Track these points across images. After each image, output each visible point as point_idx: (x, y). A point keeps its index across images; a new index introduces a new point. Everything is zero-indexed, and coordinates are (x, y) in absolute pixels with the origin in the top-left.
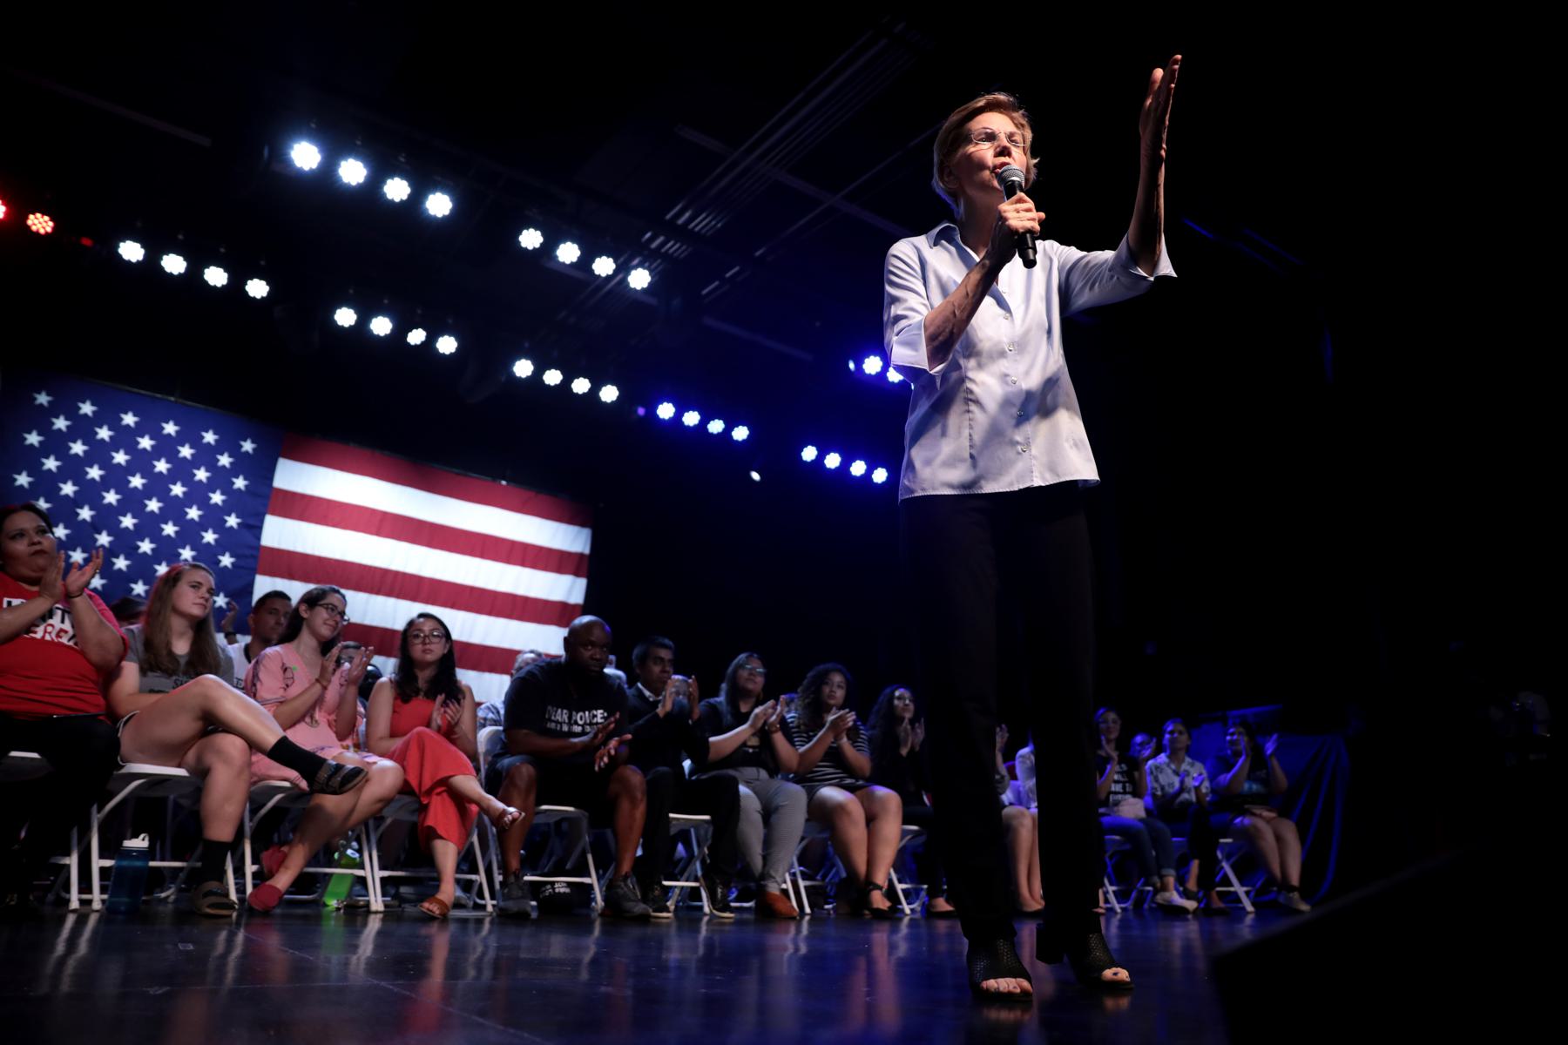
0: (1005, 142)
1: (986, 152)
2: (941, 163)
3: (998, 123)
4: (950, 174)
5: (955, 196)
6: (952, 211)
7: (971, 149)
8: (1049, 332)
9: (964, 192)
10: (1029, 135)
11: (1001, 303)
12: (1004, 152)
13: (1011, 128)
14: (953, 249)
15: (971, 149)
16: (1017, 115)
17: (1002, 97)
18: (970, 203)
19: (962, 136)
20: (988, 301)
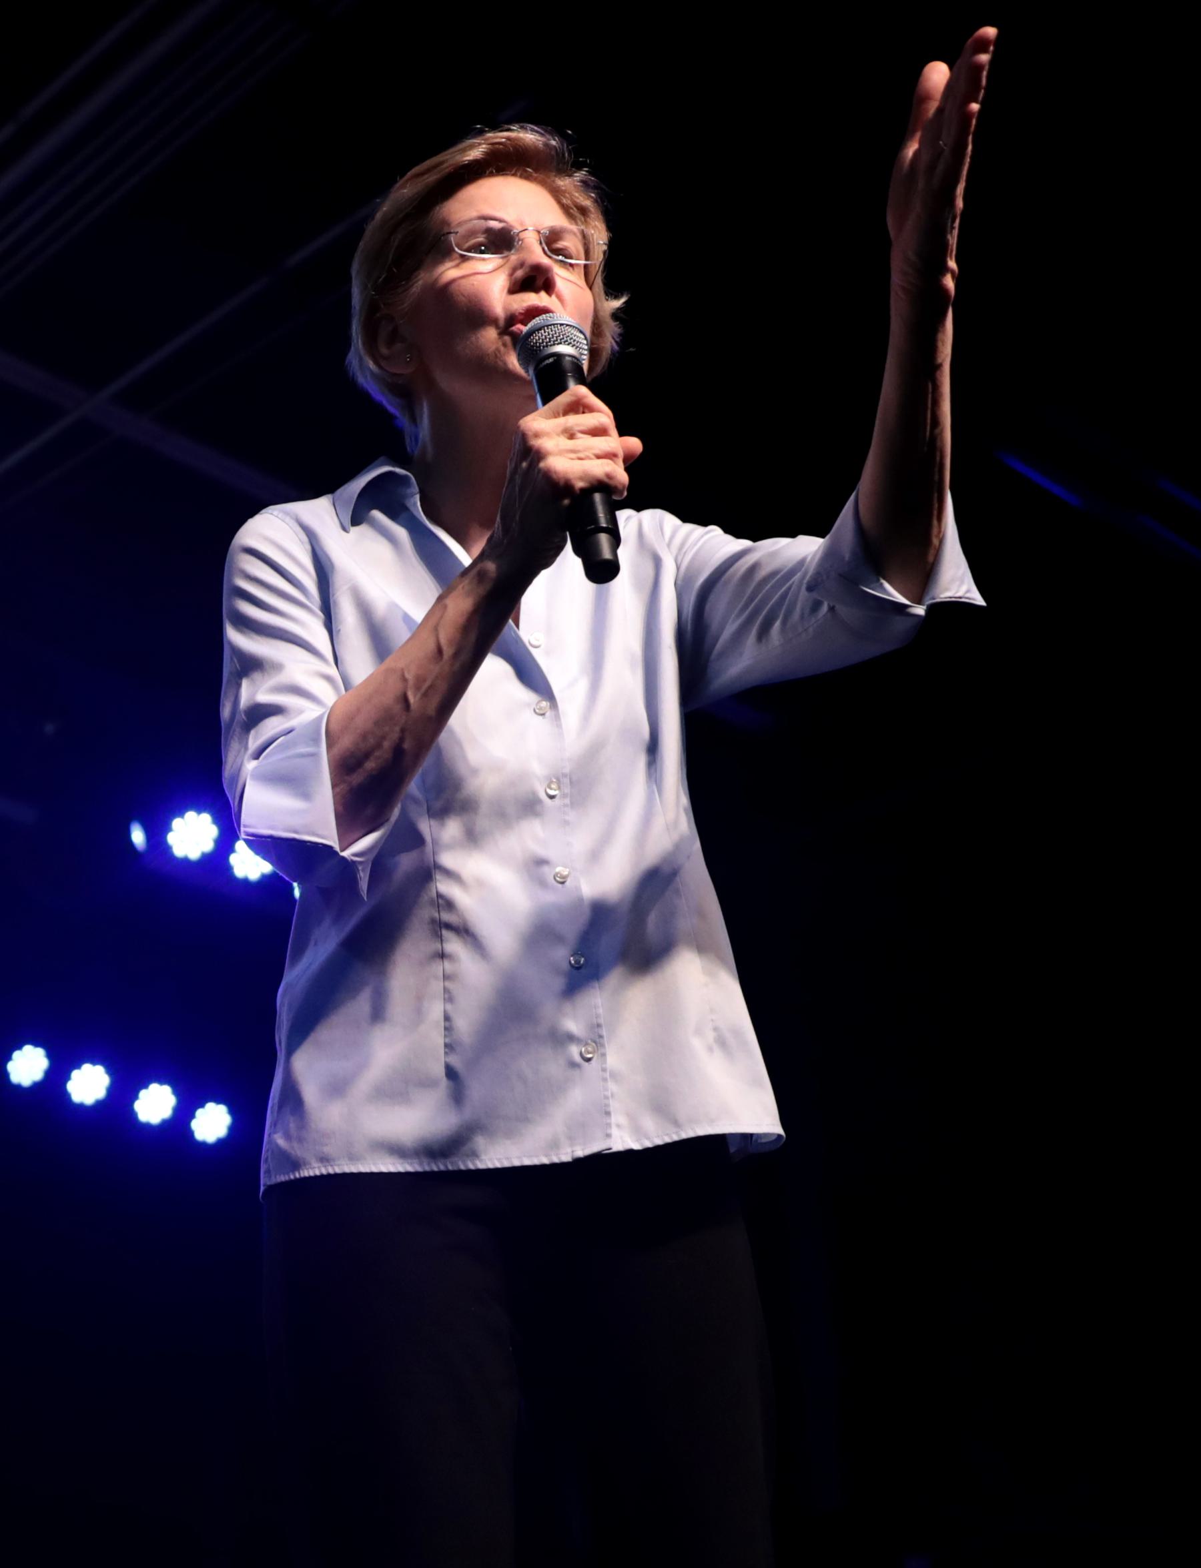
0: (538, 255)
1: (487, 279)
2: (372, 308)
3: (520, 204)
5: (406, 393)
6: (399, 434)
7: (449, 272)
10: (600, 236)
13: (553, 217)
14: (401, 533)
15: (449, 272)
16: (569, 183)
17: (529, 136)
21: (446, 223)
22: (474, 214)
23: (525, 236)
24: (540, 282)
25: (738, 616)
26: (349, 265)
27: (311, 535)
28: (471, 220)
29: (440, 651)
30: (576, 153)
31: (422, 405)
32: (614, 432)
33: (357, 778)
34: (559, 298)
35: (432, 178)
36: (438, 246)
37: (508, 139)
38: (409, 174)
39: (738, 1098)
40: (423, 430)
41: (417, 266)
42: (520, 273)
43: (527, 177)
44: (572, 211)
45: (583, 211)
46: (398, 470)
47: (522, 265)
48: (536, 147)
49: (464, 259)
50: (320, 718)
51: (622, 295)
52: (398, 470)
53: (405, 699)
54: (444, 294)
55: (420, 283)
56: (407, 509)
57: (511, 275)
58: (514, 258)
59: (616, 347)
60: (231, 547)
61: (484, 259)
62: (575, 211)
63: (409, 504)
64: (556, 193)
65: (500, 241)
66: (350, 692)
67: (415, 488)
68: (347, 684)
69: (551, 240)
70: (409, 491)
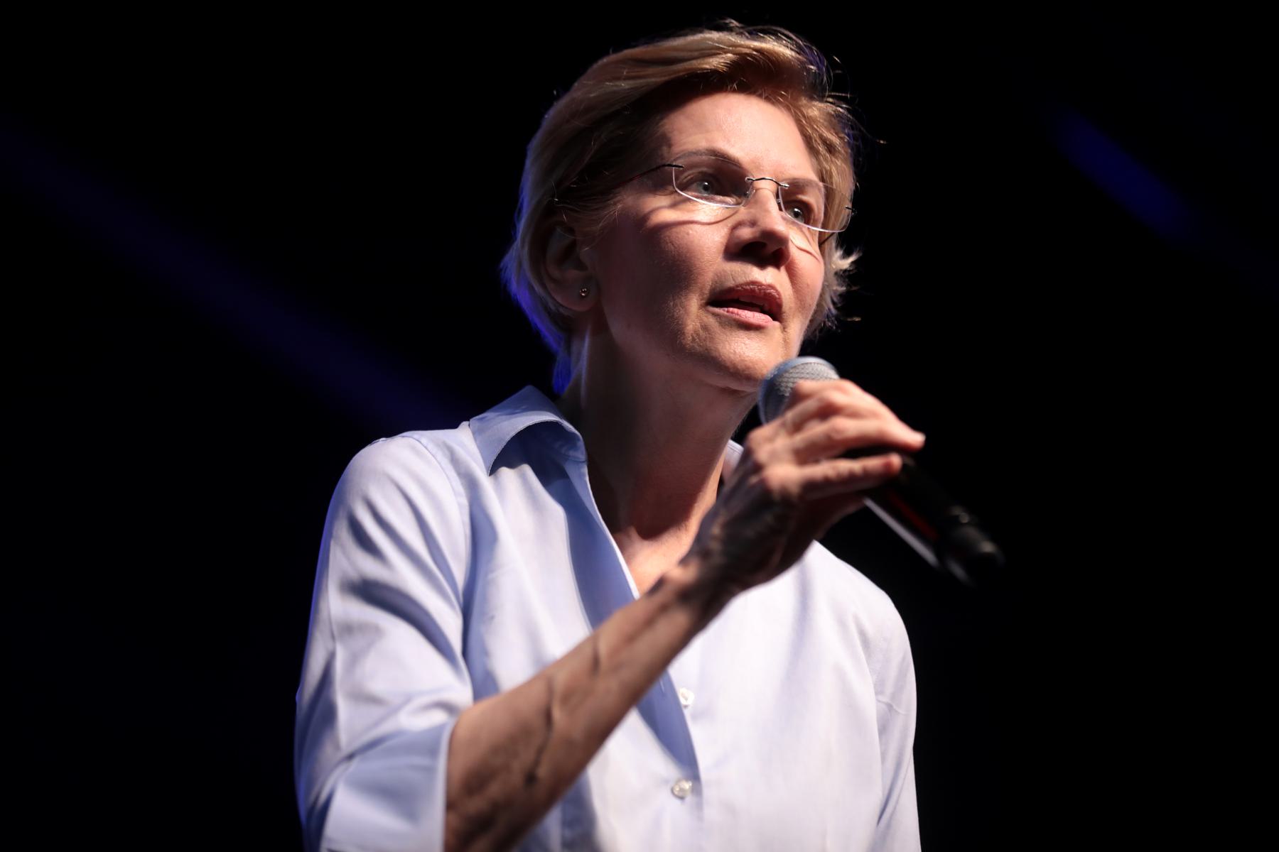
0: (777, 220)
1: (703, 223)
2: (546, 213)
3: (759, 134)
4: (569, 254)
5: (568, 327)
6: (550, 357)
7: (662, 209)
8: (734, 392)
9: (601, 327)
10: (844, 182)
11: (675, 741)
12: (766, 250)
13: (798, 165)
14: (557, 513)
15: (662, 209)
16: (817, 110)
17: (781, 48)
18: (611, 359)
19: (630, 147)
20: (633, 722)
25: (714, 51)
26: (528, 140)
27: (481, 535)
29: (595, 662)
31: (583, 339)
32: (797, 329)
33: (476, 805)
34: (792, 274)
35: (656, 76)
38: (628, 52)
40: (581, 359)
41: (622, 182)
42: (746, 233)
43: (770, 99)
45: (830, 148)
46: (566, 424)
47: (753, 223)
50: (440, 728)
51: (914, 425)
52: (566, 424)
53: (548, 716)
55: (619, 206)
56: (564, 475)
57: (735, 228)
58: (743, 212)
59: (834, 311)
61: (757, 328)
62: (821, 149)
63: (570, 470)
65: (726, 178)
66: (486, 704)
67: (581, 454)
68: (484, 685)
70: (571, 453)
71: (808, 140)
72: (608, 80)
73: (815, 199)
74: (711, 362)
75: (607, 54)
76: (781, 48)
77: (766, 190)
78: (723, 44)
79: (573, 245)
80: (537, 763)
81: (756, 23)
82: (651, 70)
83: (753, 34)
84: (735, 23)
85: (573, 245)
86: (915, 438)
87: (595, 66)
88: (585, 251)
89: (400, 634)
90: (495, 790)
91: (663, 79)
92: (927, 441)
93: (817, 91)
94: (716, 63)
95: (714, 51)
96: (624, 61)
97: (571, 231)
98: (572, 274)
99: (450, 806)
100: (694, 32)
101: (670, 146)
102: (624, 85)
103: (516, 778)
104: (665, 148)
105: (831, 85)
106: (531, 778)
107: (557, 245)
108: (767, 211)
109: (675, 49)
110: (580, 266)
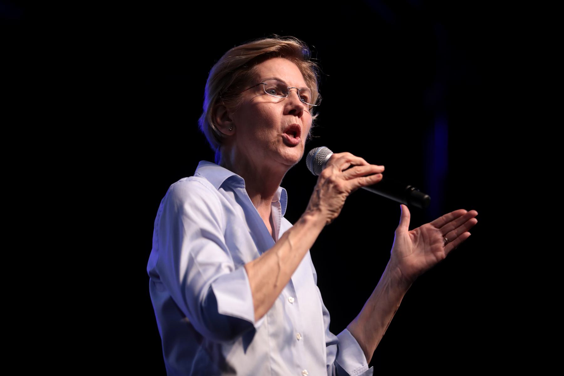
1: (274, 105)
7: (260, 99)
10: (315, 87)
12: (296, 112)
13: (302, 84)
15: (260, 99)
16: (305, 65)
17: (294, 43)
19: (244, 79)
21: (258, 75)
22: (272, 76)
23: (288, 81)
24: (297, 112)
25: (273, 45)
28: (270, 79)
30: (313, 55)
33: (260, 296)
35: (254, 54)
36: (256, 85)
37: (288, 44)
38: (241, 46)
39: (370, 171)
42: (289, 107)
43: (292, 60)
44: (306, 77)
45: (310, 77)
48: (298, 50)
49: (265, 94)
51: (379, 164)
54: (255, 108)
57: (285, 106)
58: (286, 98)
60: (169, 191)
64: (301, 68)
65: (281, 89)
69: (301, 92)
71: (304, 75)
72: (233, 56)
73: (307, 94)
74: (277, 154)
75: (233, 47)
76: (294, 43)
77: (294, 91)
78: (276, 43)
79: (226, 113)
80: (276, 281)
81: (284, 35)
82: (251, 52)
83: (286, 39)
84: (276, 36)
85: (226, 113)
86: (381, 168)
87: (231, 50)
88: (231, 116)
89: (211, 246)
90: (265, 291)
91: (257, 55)
92: (385, 168)
93: (305, 59)
94: (273, 49)
95: (273, 45)
96: (241, 49)
97: (225, 108)
98: (227, 122)
99: (253, 295)
100: (264, 39)
101: (260, 77)
102: (243, 57)
103: (271, 286)
104: (258, 78)
105: (313, 56)
106: (275, 286)
107: (220, 113)
108: (296, 99)
109: (259, 44)
110: (229, 120)
